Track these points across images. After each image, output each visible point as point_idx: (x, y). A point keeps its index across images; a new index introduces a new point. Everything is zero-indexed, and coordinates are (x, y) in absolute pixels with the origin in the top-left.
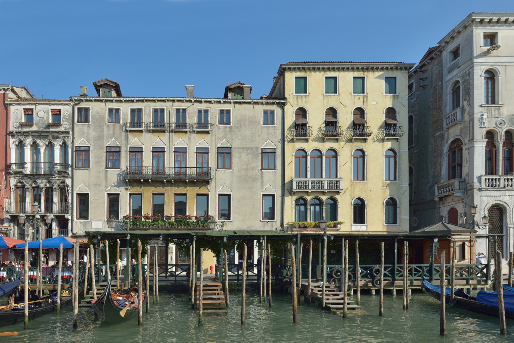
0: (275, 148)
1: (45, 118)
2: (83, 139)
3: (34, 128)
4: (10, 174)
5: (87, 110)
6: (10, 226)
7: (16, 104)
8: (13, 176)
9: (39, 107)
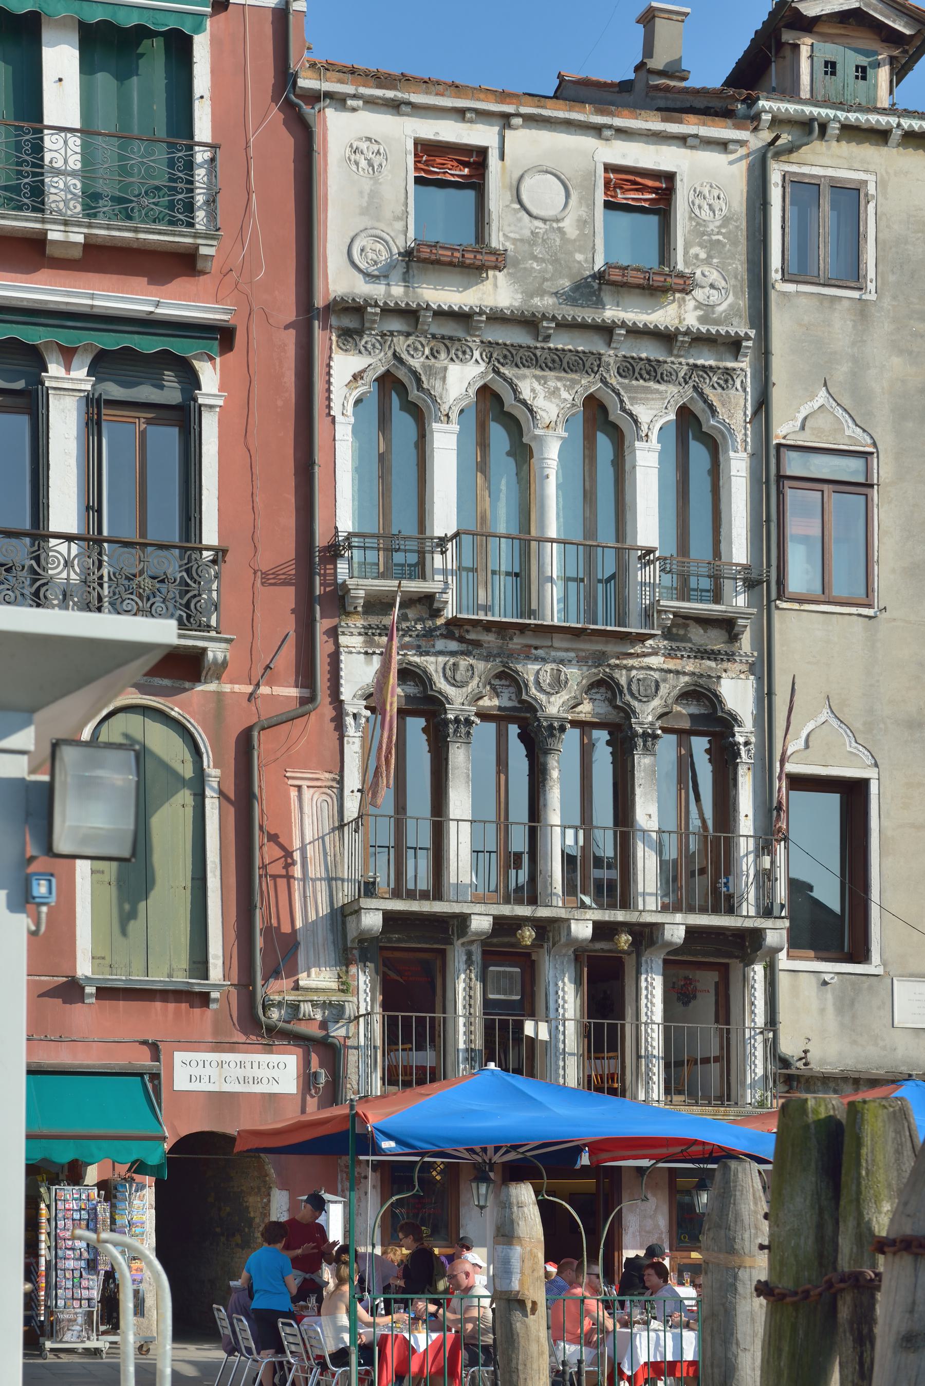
0: (865, 455)
1: (569, 225)
2: (822, 397)
3: (497, 293)
4: (339, 601)
5: (850, 197)
6: (345, 987)
7: (371, 103)
8: (358, 622)
9: (526, 145)
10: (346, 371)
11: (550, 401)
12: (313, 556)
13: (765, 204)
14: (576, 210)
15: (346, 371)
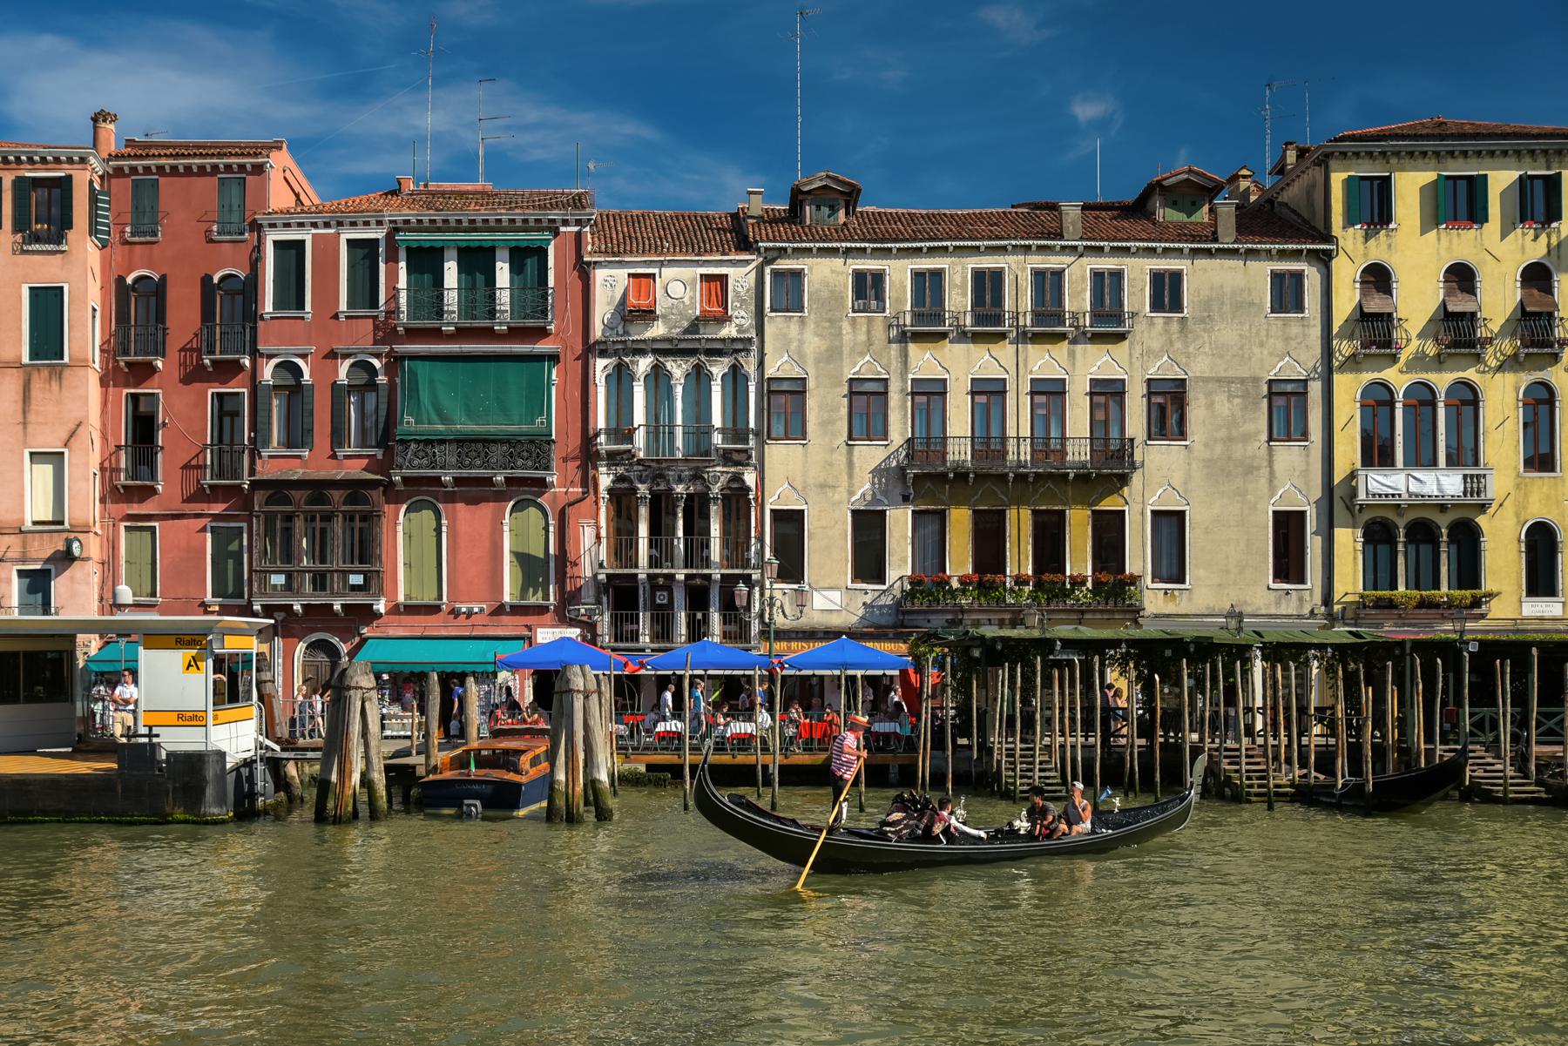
1: (686, 300)
3: (658, 330)
5: (798, 275)
10: (601, 366)
11: (678, 369)
12: (588, 439)
13: (763, 283)
14: (689, 293)
15: (601, 366)
